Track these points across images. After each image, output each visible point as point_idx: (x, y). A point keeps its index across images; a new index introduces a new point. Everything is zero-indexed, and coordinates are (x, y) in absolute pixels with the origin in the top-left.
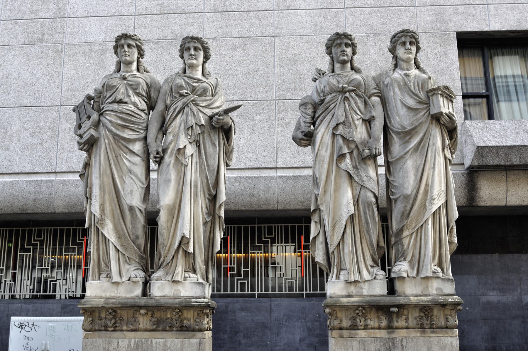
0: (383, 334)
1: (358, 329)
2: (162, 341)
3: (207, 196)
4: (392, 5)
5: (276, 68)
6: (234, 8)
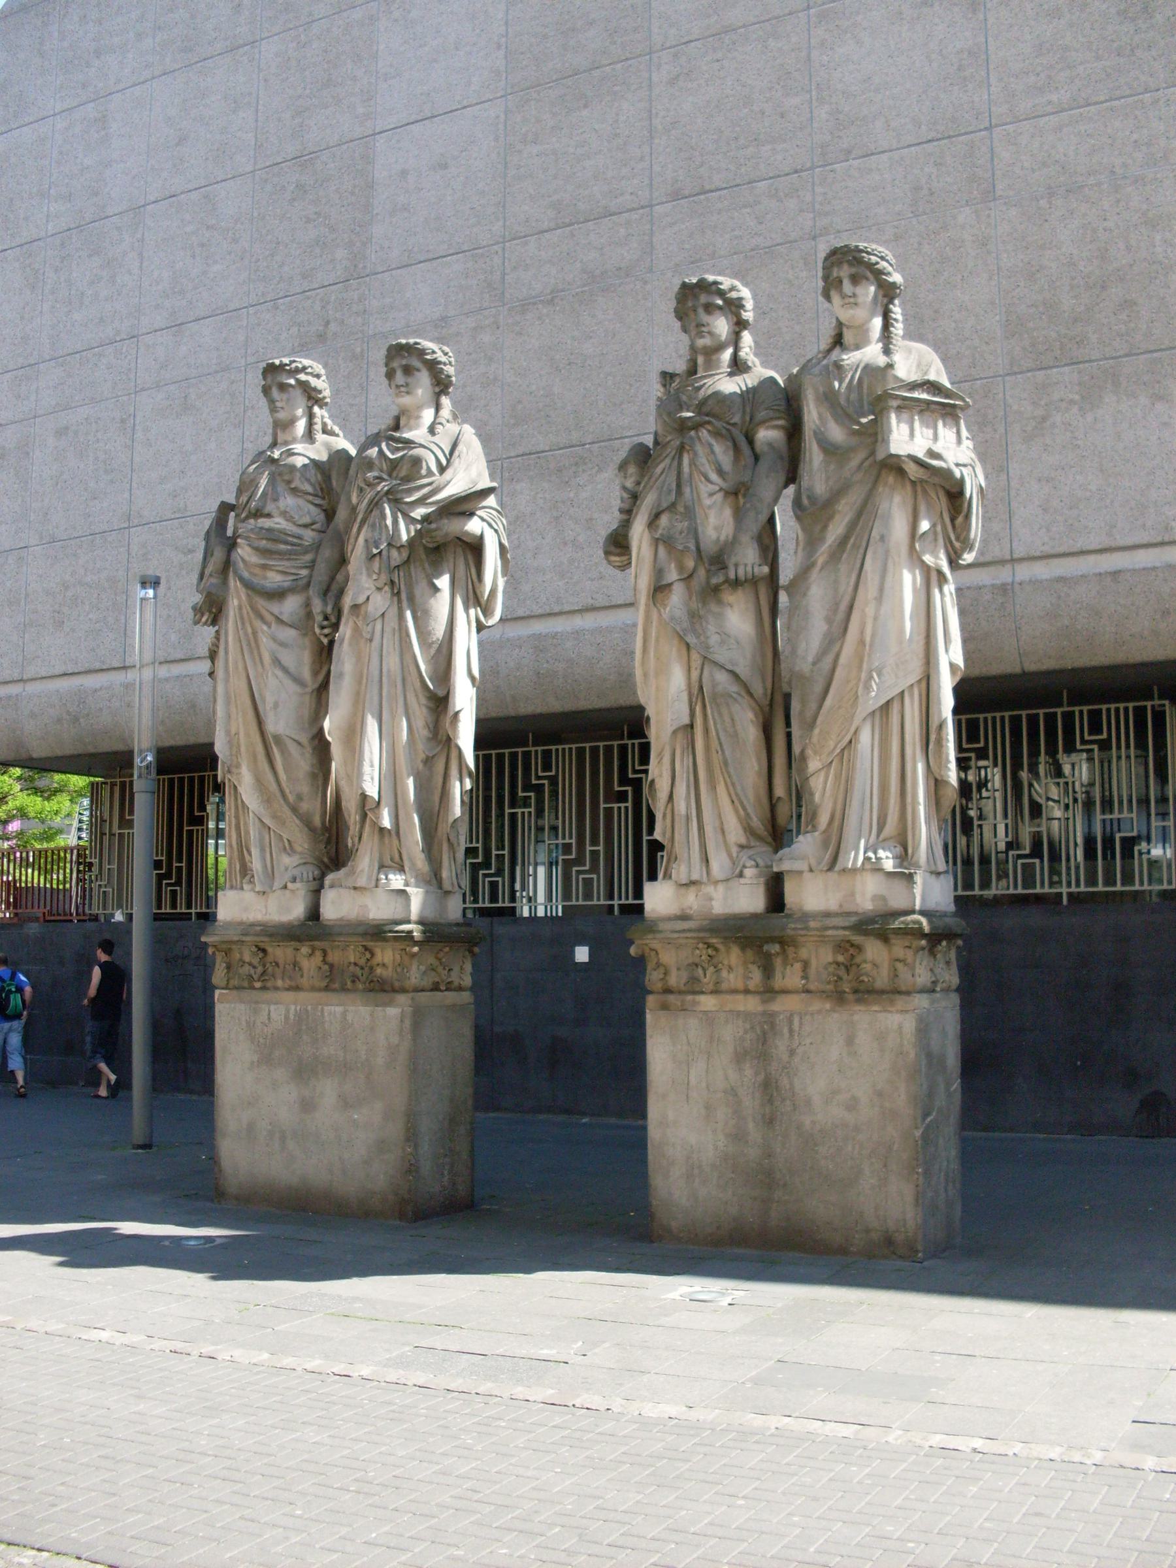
0: (752, 1004)
1: (702, 993)
2: (339, 1009)
4: (1118, 93)
5: (821, 320)
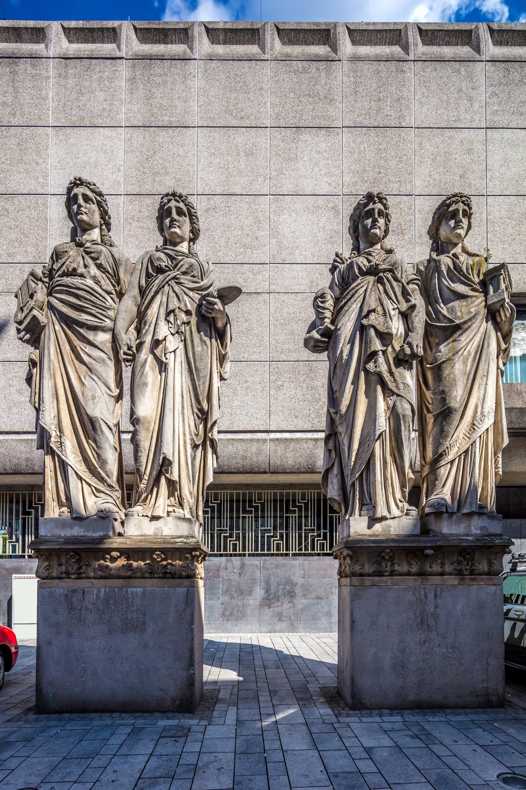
3: (196, 411)
6: (227, 260)
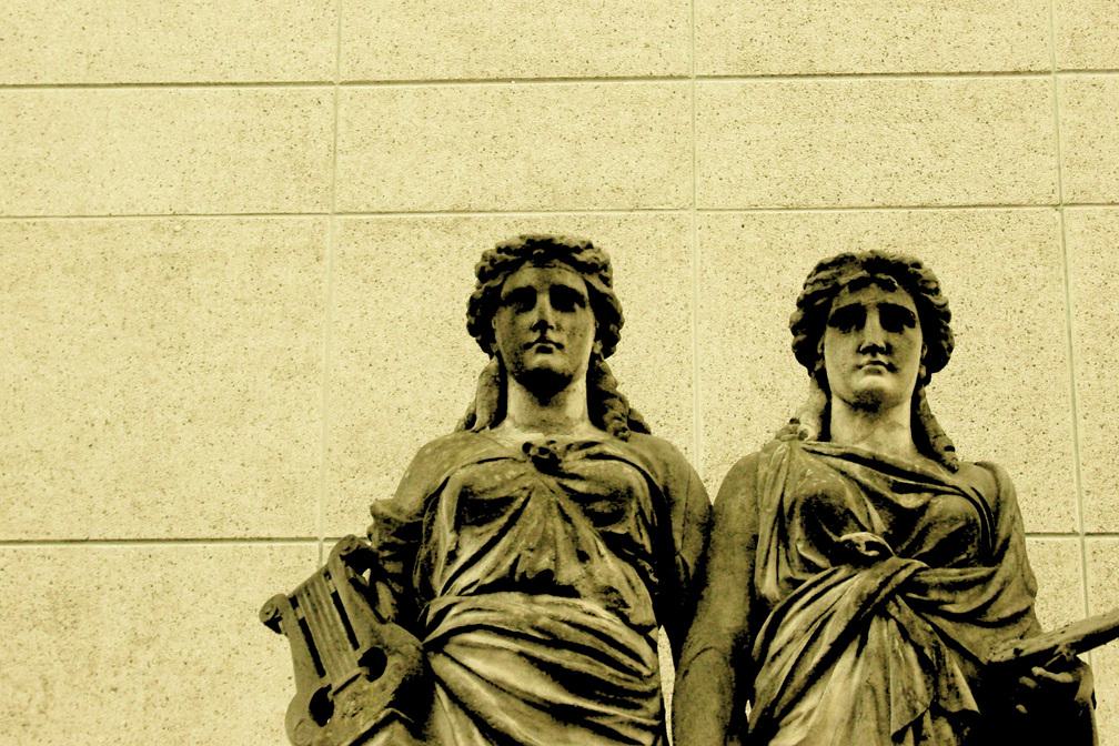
5: (1079, 369)
6: (845, 59)
